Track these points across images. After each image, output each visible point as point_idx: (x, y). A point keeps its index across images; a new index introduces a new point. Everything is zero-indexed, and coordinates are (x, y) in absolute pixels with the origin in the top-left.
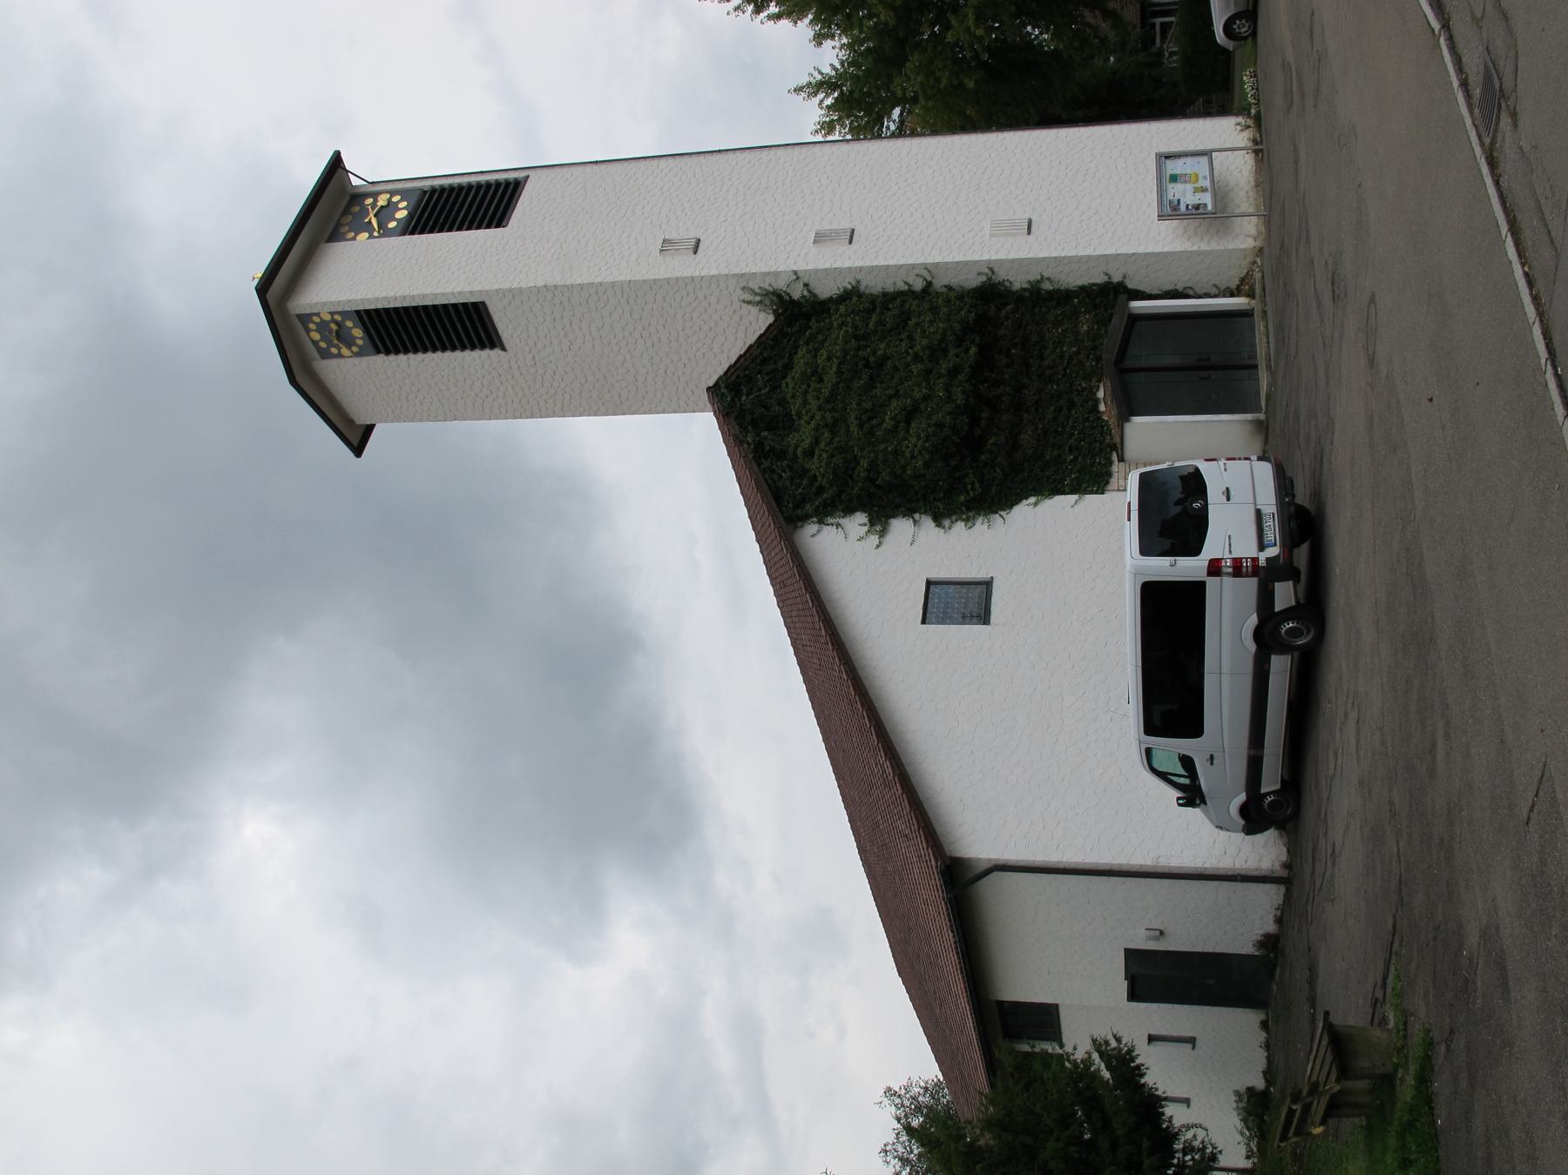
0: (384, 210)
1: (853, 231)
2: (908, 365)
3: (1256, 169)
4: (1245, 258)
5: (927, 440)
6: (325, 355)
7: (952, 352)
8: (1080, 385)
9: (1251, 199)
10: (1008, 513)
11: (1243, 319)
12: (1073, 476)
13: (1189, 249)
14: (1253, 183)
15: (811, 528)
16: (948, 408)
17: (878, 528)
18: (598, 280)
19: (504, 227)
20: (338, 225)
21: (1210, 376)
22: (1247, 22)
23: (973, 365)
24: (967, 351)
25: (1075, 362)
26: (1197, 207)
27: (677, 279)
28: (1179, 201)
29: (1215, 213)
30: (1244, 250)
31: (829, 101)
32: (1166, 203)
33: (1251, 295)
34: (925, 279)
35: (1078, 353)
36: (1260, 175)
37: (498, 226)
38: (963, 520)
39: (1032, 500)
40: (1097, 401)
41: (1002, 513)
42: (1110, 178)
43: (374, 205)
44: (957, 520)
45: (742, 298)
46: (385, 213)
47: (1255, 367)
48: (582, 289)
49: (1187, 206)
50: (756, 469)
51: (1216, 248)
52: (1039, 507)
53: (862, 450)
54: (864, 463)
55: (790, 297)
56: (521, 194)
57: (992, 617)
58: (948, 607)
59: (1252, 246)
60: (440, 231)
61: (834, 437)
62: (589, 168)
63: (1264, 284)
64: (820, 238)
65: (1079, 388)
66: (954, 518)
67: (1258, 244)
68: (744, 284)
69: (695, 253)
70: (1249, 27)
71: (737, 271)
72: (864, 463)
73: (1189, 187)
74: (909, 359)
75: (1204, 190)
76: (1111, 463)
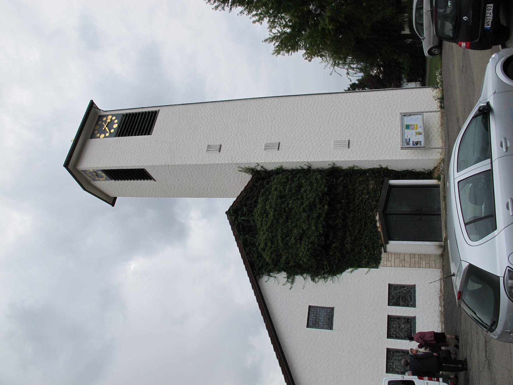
0: (110, 123)
1: (279, 143)
2: (300, 213)
3: (441, 116)
4: (436, 161)
5: (308, 251)
6: (94, 180)
7: (318, 206)
8: (369, 214)
9: (439, 132)
10: (340, 276)
11: (435, 188)
12: (366, 260)
13: (413, 158)
14: (440, 124)
15: (265, 278)
16: (316, 234)
17: (290, 280)
18: (184, 163)
19: (150, 135)
20: (94, 130)
21: (421, 218)
22: (438, 49)
23: (326, 212)
24: (324, 206)
25: (367, 203)
26: (417, 143)
27: (213, 164)
28: (409, 139)
29: (425, 147)
30: (436, 159)
31: (277, 44)
32: (404, 141)
33: (439, 179)
34: (308, 166)
35: (368, 199)
36: (443, 119)
37: (149, 134)
38: (323, 278)
39: (350, 270)
40: (376, 221)
41: (338, 275)
42: (381, 119)
43: (106, 121)
44: (320, 278)
45: (238, 170)
46: (110, 125)
47: (440, 215)
48: (178, 166)
49: (413, 142)
50: (244, 252)
51: (425, 158)
52: (353, 273)
53: (283, 251)
54: (284, 257)
55: (257, 170)
56: (157, 117)
57: (334, 326)
58: (315, 324)
59: (439, 158)
60: (128, 136)
61: (272, 245)
62: (181, 106)
63: (445, 181)
64: (267, 147)
65: (369, 215)
66: (319, 277)
67: (442, 157)
68: (239, 166)
69: (220, 152)
70: (439, 51)
71: (235, 162)
72: (284, 257)
73: (414, 131)
74: (301, 210)
75: (420, 134)
76: (380, 253)
